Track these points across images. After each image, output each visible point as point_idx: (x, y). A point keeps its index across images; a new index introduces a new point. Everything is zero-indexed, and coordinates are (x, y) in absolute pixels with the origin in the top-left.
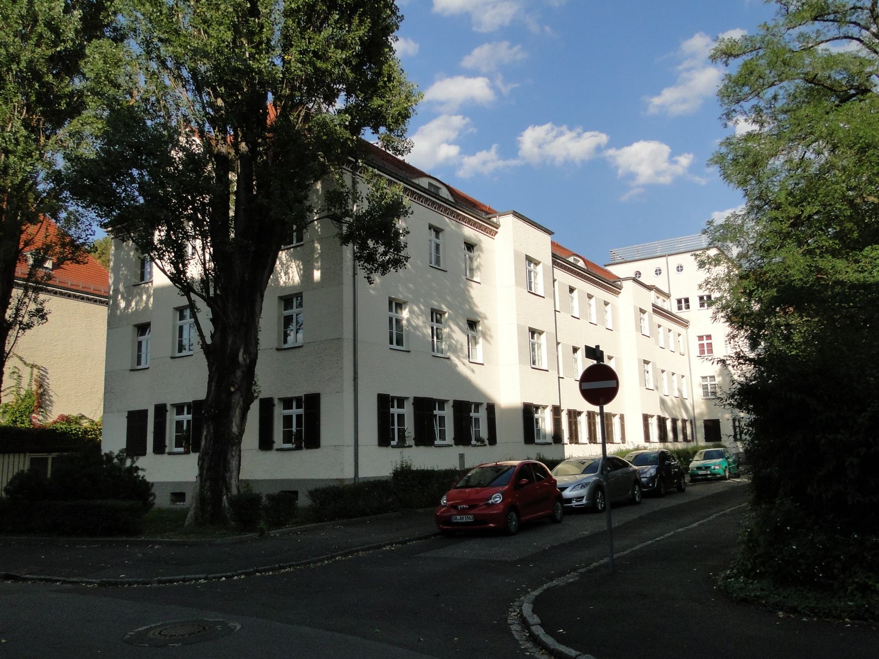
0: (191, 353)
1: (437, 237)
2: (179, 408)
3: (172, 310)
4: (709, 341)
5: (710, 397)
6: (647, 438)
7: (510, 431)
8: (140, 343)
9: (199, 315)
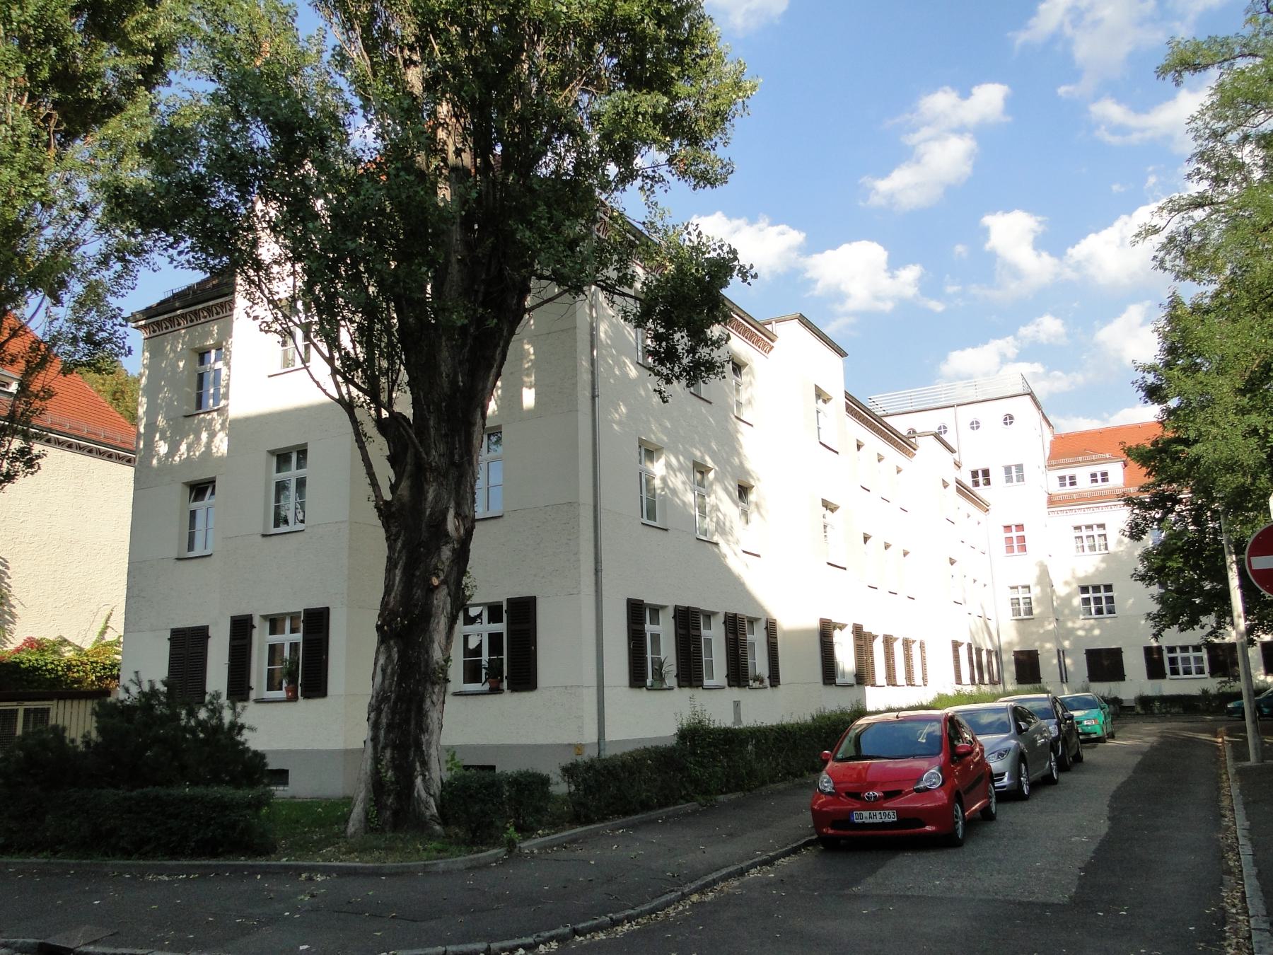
0: (300, 526)
2: (275, 623)
3: (264, 455)
4: (1021, 534)
5: (1023, 616)
6: (959, 679)
7: (799, 667)
8: (193, 514)
9: (369, 448)
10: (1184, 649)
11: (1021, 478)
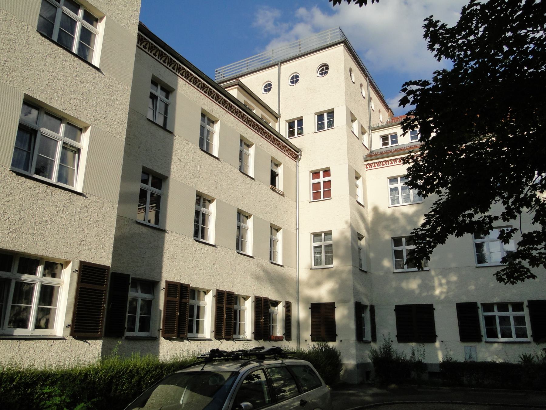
1: (167, 97)
10: (503, 307)
11: (331, 124)
